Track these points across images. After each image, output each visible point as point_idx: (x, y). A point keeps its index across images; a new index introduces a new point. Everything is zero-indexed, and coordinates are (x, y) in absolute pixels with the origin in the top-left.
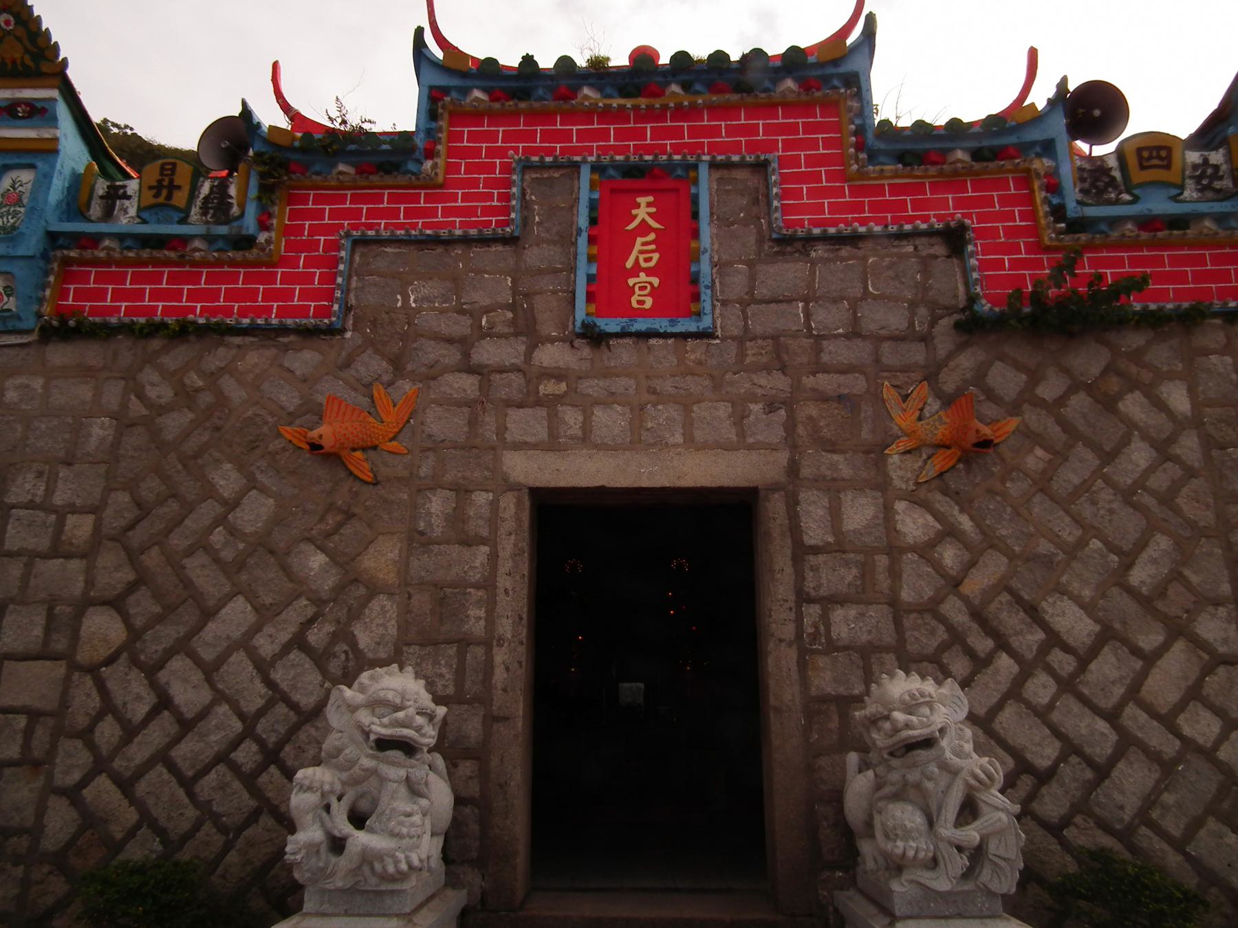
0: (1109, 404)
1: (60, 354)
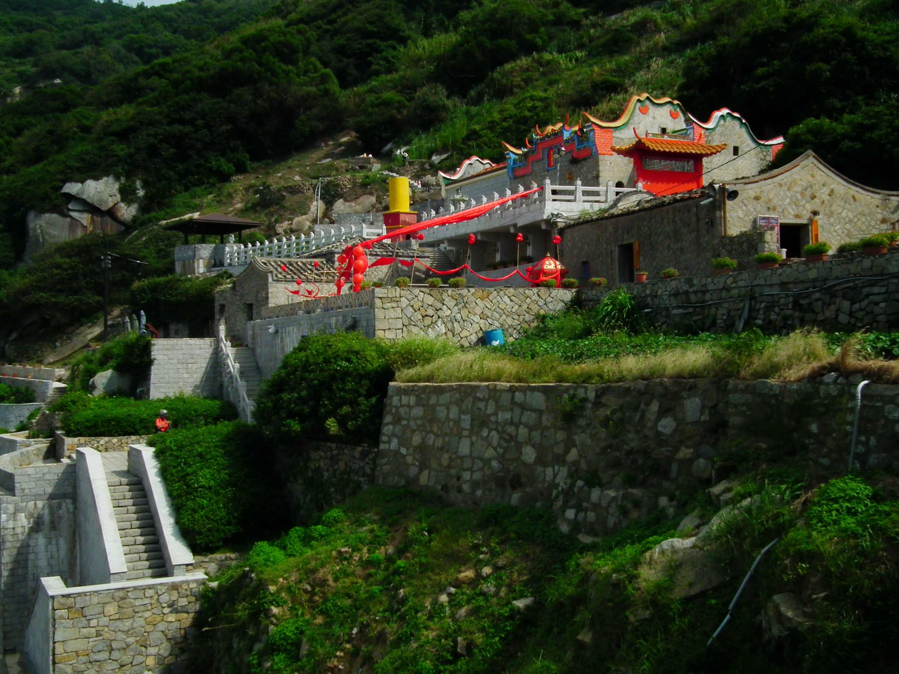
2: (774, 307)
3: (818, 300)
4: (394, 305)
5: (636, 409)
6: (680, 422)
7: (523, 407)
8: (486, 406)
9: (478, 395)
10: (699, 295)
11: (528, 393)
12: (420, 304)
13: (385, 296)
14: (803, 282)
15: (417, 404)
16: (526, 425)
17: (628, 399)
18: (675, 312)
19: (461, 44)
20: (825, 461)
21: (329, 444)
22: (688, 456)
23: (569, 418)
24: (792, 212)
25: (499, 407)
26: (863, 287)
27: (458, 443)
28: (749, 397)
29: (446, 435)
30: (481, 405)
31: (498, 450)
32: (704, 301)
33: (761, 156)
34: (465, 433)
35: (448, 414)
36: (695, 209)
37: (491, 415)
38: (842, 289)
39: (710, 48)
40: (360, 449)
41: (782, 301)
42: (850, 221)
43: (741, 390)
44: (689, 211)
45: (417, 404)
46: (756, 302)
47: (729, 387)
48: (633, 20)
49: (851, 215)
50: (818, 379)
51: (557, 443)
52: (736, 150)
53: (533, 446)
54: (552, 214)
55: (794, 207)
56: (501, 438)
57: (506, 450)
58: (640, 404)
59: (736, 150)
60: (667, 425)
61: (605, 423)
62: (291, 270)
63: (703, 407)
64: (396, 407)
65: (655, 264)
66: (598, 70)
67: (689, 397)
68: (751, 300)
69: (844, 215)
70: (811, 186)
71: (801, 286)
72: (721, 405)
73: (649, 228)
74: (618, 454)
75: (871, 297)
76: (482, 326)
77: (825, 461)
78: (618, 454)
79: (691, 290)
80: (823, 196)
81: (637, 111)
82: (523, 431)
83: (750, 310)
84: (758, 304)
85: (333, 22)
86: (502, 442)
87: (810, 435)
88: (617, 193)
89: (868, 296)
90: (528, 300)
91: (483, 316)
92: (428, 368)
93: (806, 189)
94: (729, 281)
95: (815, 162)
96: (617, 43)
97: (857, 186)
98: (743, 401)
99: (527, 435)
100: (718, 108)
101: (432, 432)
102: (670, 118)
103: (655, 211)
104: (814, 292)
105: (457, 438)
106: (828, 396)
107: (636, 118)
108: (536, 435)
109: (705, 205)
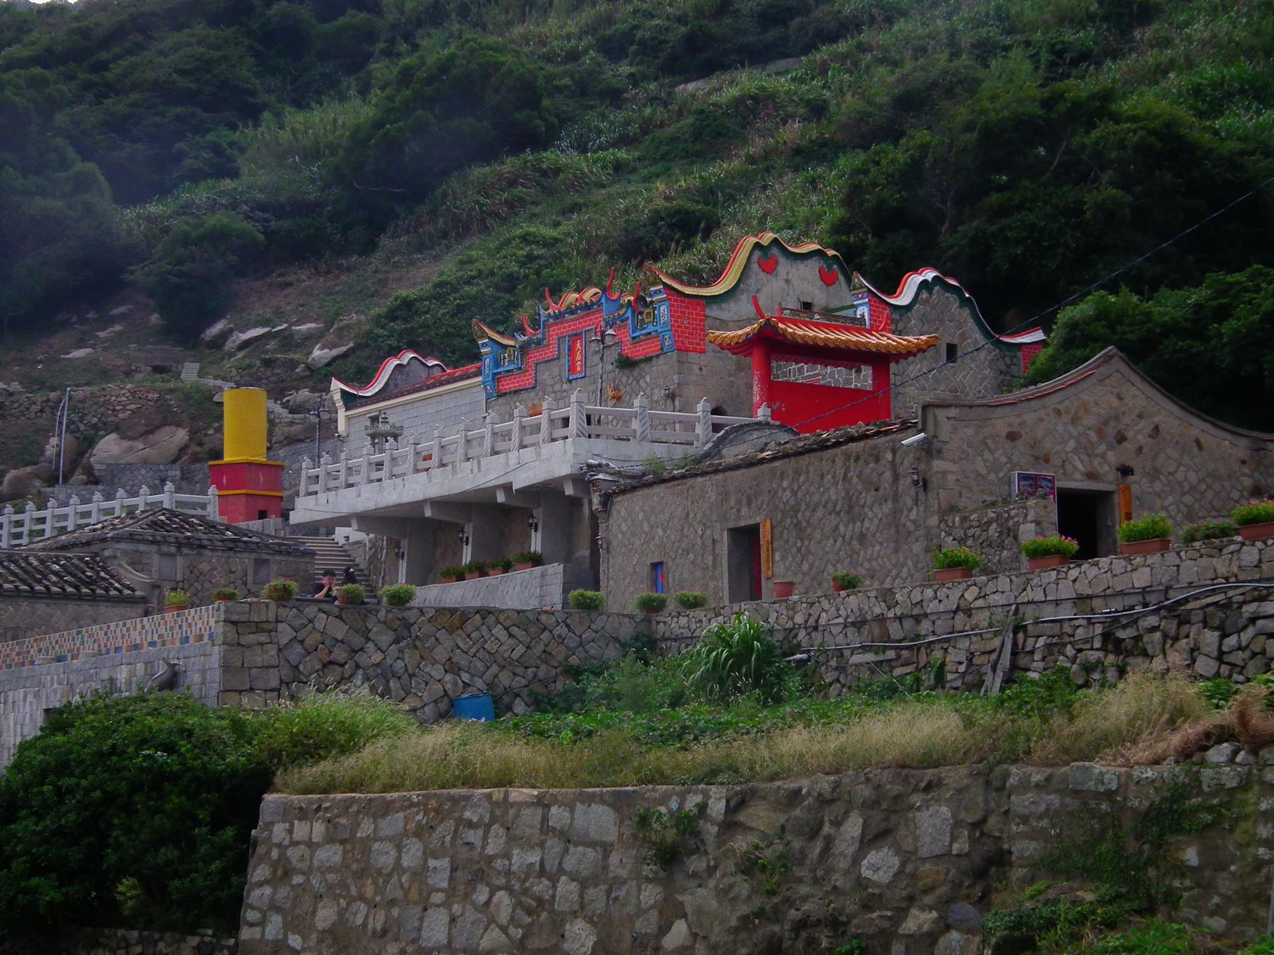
0: (638, 382)
1: (501, 400)
2: (1065, 645)
3: (1153, 629)
4: (263, 638)
5: (813, 832)
6: (907, 857)
7: (568, 838)
8: (485, 838)
9: (467, 814)
10: (908, 624)
11: (579, 807)
12: (318, 636)
13: (244, 618)
14: (1122, 593)
15: (329, 840)
16: (573, 877)
17: (797, 812)
18: (856, 659)
19: (378, 125)
20: (1217, 923)
21: (120, 932)
22: (926, 928)
23: (669, 857)
24: (1080, 466)
25: (513, 840)
26: (1244, 602)
27: (421, 919)
28: (1054, 799)
29: (393, 903)
30: (473, 836)
31: (512, 930)
32: (918, 637)
33: (1001, 365)
34: (438, 898)
35: (399, 858)
36: (889, 456)
37: (496, 856)
38: (1202, 608)
39: (897, 155)
40: (194, 941)
41: (1080, 633)
42: (1193, 489)
43: (1037, 785)
44: (877, 460)
45: (329, 840)
46: (1026, 636)
47: (1012, 781)
48: (734, 92)
49: (1193, 477)
50: (1196, 758)
51: (640, 912)
52: (952, 351)
53: (590, 920)
54: (590, 466)
55: (1084, 457)
56: (519, 904)
57: (528, 932)
58: (821, 824)
59: (952, 351)
60: (880, 865)
61: (749, 866)
62: (15, 575)
63: (957, 824)
64: (279, 845)
65: (805, 566)
66: (660, 193)
67: (927, 805)
68: (1015, 632)
69: (1180, 476)
70: (1117, 418)
71: (1116, 604)
72: (993, 822)
73: (794, 493)
74: (776, 928)
75: (1260, 623)
76: (448, 687)
77: (1217, 923)
78: (776, 928)
79: (891, 614)
80: (1140, 437)
81: (755, 267)
82: (566, 887)
83: (1014, 653)
84: (1031, 641)
85: (101, 67)
86: (519, 911)
87: (1182, 870)
88: (716, 428)
89: (1253, 620)
90: (545, 636)
91: (452, 668)
92: (350, 762)
93: (1106, 423)
94: (969, 596)
95: (1124, 368)
96: (711, 134)
97: (1205, 420)
98: (1042, 808)
99: (575, 897)
100: (916, 270)
101: (362, 898)
102: (820, 283)
103: (806, 459)
104: (1145, 615)
105: (419, 909)
106: (1220, 789)
107: (752, 281)
108: (596, 895)
109: (908, 446)
